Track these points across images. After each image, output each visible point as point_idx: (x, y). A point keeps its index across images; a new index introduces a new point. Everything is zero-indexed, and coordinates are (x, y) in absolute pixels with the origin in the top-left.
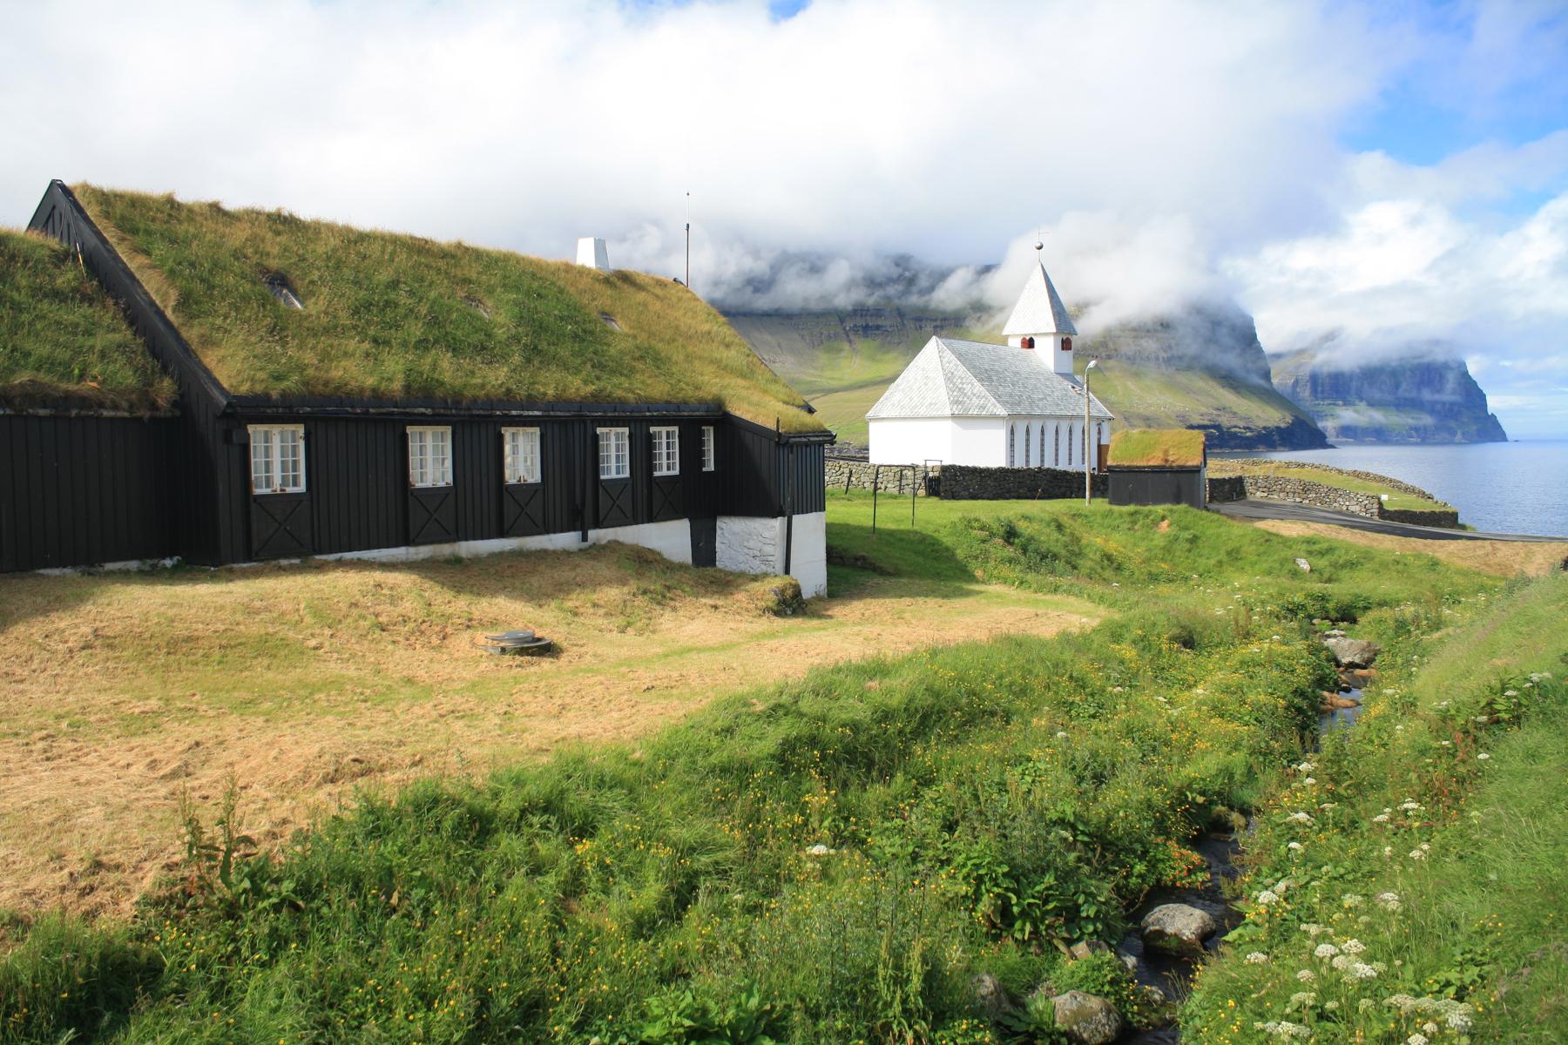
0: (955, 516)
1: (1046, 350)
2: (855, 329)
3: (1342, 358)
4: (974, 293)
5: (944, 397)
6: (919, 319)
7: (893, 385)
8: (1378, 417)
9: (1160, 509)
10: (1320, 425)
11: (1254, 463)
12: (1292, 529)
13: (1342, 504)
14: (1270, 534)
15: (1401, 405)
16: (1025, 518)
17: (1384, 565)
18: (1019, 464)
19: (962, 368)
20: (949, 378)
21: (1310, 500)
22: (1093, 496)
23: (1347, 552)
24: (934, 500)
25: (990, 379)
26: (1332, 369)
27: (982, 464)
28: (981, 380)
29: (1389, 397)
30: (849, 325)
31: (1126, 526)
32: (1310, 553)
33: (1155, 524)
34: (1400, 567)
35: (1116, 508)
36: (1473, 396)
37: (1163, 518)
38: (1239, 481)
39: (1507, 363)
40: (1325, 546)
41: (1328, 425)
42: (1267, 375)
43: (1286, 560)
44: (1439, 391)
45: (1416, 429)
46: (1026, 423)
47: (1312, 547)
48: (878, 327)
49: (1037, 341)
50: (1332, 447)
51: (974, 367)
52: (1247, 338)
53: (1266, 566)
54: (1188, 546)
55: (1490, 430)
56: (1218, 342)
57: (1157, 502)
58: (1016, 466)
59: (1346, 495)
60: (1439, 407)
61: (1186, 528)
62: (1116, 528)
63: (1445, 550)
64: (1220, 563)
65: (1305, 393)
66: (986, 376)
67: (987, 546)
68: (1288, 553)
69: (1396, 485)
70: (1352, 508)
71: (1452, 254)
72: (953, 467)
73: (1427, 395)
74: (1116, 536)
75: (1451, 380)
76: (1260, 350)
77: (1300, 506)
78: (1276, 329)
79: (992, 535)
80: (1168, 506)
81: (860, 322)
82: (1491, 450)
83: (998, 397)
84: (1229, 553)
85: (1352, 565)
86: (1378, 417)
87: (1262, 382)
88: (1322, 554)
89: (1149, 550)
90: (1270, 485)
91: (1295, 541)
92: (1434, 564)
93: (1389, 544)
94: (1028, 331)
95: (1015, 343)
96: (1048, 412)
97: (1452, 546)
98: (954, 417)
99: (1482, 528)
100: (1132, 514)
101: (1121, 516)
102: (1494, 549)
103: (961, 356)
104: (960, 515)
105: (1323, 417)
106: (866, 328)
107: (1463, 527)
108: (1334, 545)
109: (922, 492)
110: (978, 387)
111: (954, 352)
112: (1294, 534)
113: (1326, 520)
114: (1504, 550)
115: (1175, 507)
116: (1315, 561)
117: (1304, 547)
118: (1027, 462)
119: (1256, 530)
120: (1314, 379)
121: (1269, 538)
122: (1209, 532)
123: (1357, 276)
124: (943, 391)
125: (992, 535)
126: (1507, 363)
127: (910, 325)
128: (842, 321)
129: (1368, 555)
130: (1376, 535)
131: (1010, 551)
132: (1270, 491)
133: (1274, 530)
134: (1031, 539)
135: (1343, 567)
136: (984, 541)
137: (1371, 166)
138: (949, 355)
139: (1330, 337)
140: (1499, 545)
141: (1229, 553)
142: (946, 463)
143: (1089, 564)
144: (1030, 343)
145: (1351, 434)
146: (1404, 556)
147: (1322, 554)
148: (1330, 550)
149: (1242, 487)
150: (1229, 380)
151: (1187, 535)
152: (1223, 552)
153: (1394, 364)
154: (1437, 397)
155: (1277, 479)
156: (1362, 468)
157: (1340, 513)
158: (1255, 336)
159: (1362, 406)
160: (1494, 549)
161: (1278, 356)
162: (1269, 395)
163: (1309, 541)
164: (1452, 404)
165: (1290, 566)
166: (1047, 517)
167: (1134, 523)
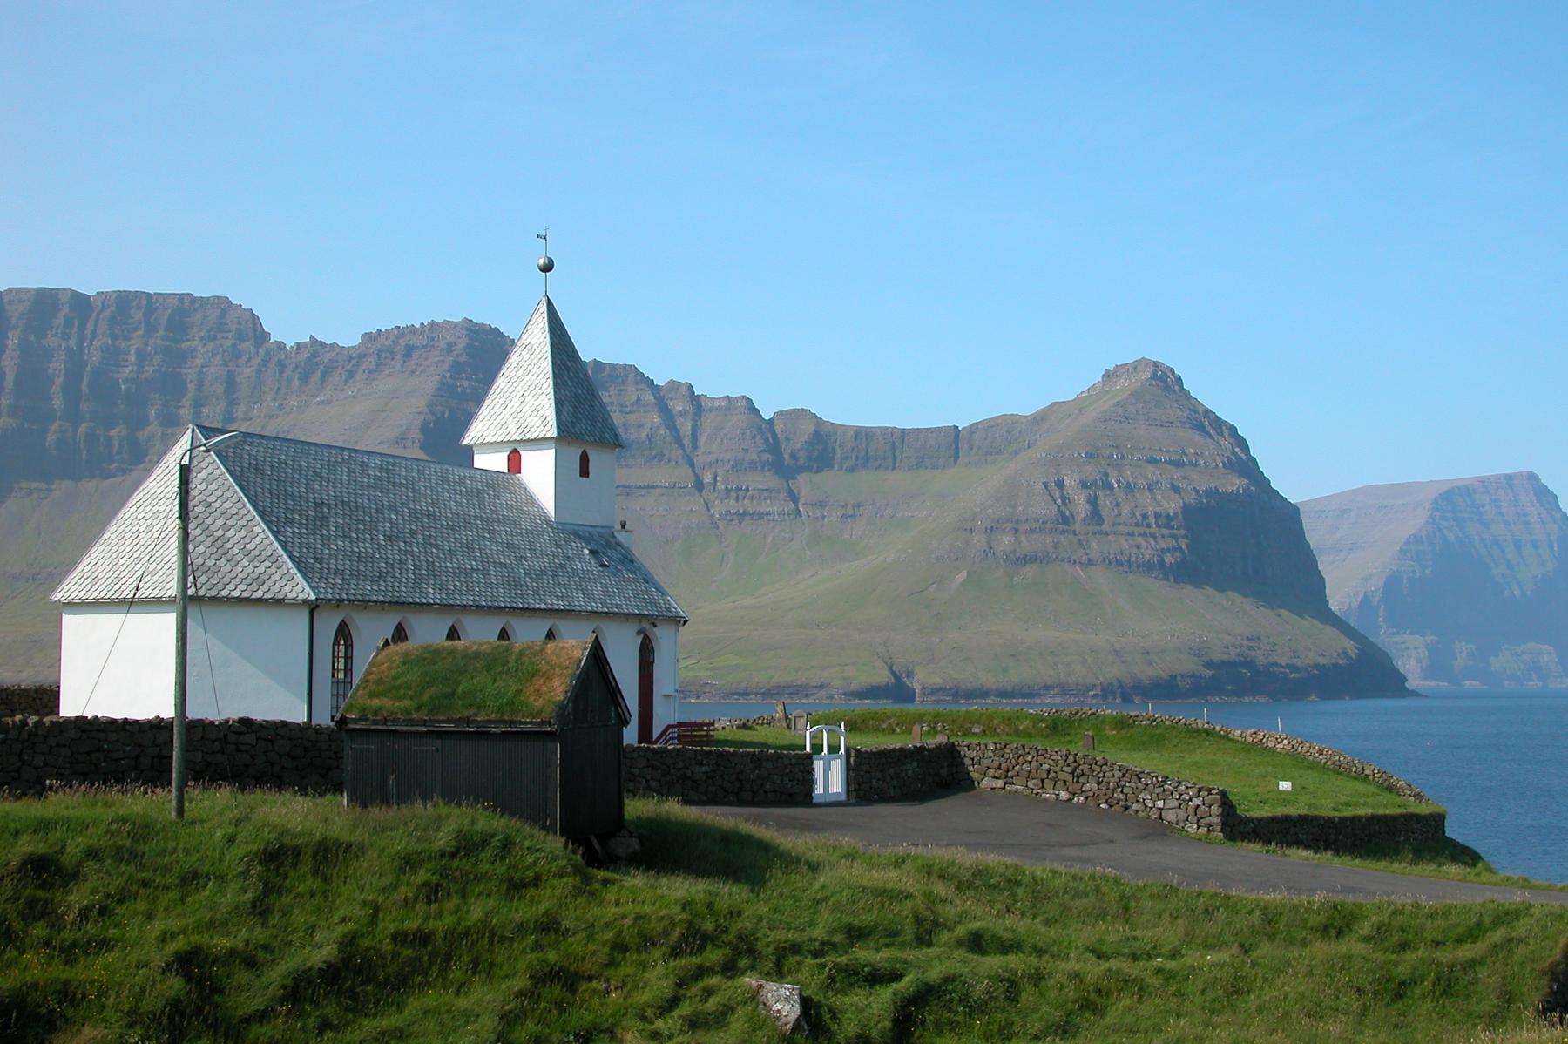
1: (540, 475)
69: (1298, 761)
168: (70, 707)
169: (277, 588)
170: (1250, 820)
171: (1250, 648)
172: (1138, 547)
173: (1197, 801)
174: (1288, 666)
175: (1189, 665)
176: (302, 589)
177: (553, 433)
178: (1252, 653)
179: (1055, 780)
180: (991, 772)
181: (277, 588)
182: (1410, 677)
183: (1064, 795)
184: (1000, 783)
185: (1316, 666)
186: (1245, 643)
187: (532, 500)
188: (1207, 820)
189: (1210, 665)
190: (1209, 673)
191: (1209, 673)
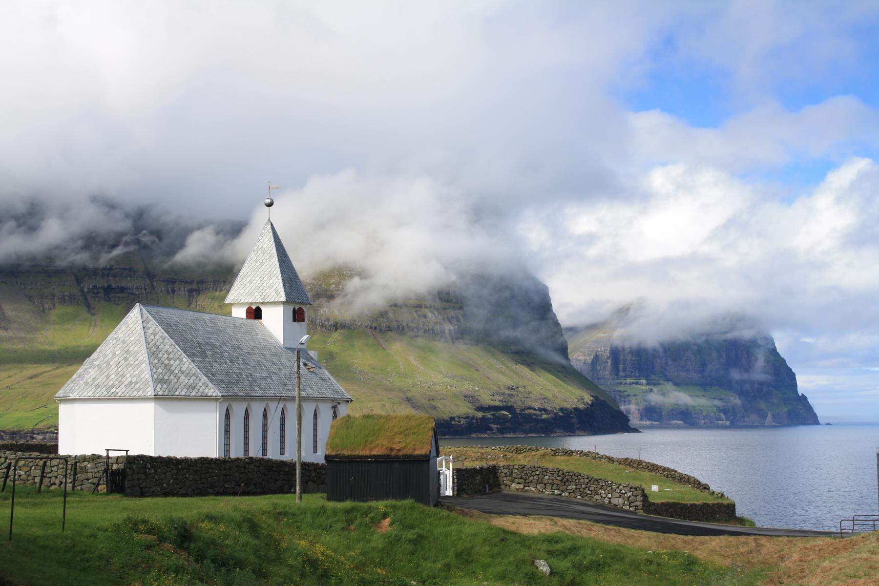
0: (119, 517)
1: (274, 321)
2: (95, 291)
3: (647, 332)
4: (216, 256)
5: (147, 375)
6: (172, 281)
7: (88, 361)
8: (682, 398)
9: (381, 505)
10: (623, 408)
11: (518, 451)
12: (534, 526)
13: (604, 496)
14: (505, 532)
15: (705, 384)
16: (210, 518)
17: (636, 566)
18: (236, 453)
19: (169, 341)
20: (153, 353)
21: (574, 493)
22: (304, 490)
23: (593, 550)
24: (117, 496)
25: (203, 354)
26: (634, 343)
27: (179, 454)
28: (191, 356)
29: (695, 376)
30: (87, 285)
31: (340, 525)
32: (551, 553)
33: (376, 521)
34: (653, 568)
35: (331, 504)
36: (782, 375)
37: (385, 516)
38: (493, 471)
39: (808, 340)
40: (569, 544)
41: (632, 409)
42: (563, 350)
43: (524, 562)
44: (747, 371)
45: (725, 411)
46: (243, 406)
47: (553, 546)
48: (122, 290)
49: (265, 311)
50: (635, 430)
51: (185, 340)
52: (542, 308)
53: (499, 569)
54: (410, 547)
55: (800, 412)
56: (508, 313)
57: (378, 498)
58: (233, 456)
59: (609, 486)
60: (747, 387)
61: (412, 527)
62: (328, 528)
63: (708, 549)
64: (448, 567)
65: (606, 371)
66: (198, 350)
67: (152, 553)
68: (525, 554)
69: (670, 475)
70: (615, 501)
71: (731, 223)
72: (142, 457)
73: (736, 375)
74: (327, 538)
75: (760, 362)
76: (556, 324)
77: (558, 499)
78: (572, 297)
79: (162, 539)
80: (392, 502)
81: (101, 283)
82: (802, 434)
83: (211, 376)
84: (458, 555)
85: (598, 566)
86: (682, 398)
87: (558, 358)
88: (565, 554)
89: (364, 553)
90: (527, 475)
91: (535, 539)
92: (690, 563)
93: (645, 542)
94: (255, 299)
95: (239, 313)
96: (271, 393)
97: (715, 542)
98: (157, 398)
99: (762, 522)
100: (347, 512)
101: (335, 512)
102: (758, 545)
103: (169, 328)
104: (124, 515)
105: (626, 398)
106: (108, 290)
107: (741, 521)
108: (578, 544)
109: (102, 488)
110: (187, 364)
111: (160, 322)
112: (535, 532)
113: (579, 515)
114: (768, 546)
115: (399, 503)
116: (555, 562)
117: (545, 546)
118: (246, 450)
119: (491, 528)
120: (616, 354)
121: (505, 536)
122: (437, 531)
123: (651, 245)
124: (145, 366)
125: (162, 539)
126: (808, 340)
127: (161, 287)
128: (79, 282)
129: (616, 556)
130: (633, 532)
131: (181, 559)
132: (527, 483)
133: (513, 528)
134: (212, 543)
135: (588, 568)
136: (149, 547)
137: (649, 126)
138: (154, 326)
139: (623, 312)
140: (763, 541)
141: (458, 555)
142: (133, 452)
143: (285, 571)
144: (255, 313)
145: (656, 416)
146: (659, 555)
147: (565, 554)
148: (574, 550)
149: (496, 478)
150: (524, 356)
151: (410, 534)
152: (451, 554)
153: (700, 341)
154: (745, 376)
155: (534, 469)
156: (633, 456)
157: (601, 506)
158: (550, 306)
159: (669, 386)
160: (758, 545)
161: (572, 330)
162: (567, 373)
163: (551, 540)
164: (761, 384)
165: (527, 569)
166: (238, 516)
167: (349, 522)
168: (62, 451)
169: (201, 390)
170: (654, 504)
171: (511, 395)
172: (425, 317)
173: (629, 494)
174: (540, 410)
175: (464, 409)
176: (213, 391)
177: (283, 299)
178: (513, 400)
179: (552, 484)
180: (517, 480)
181: (201, 390)
182: (631, 417)
183: (557, 492)
184: (521, 486)
185: (561, 409)
186: (507, 392)
187: (271, 337)
188: (636, 504)
189: (481, 409)
190: (480, 415)
191: (480, 415)
